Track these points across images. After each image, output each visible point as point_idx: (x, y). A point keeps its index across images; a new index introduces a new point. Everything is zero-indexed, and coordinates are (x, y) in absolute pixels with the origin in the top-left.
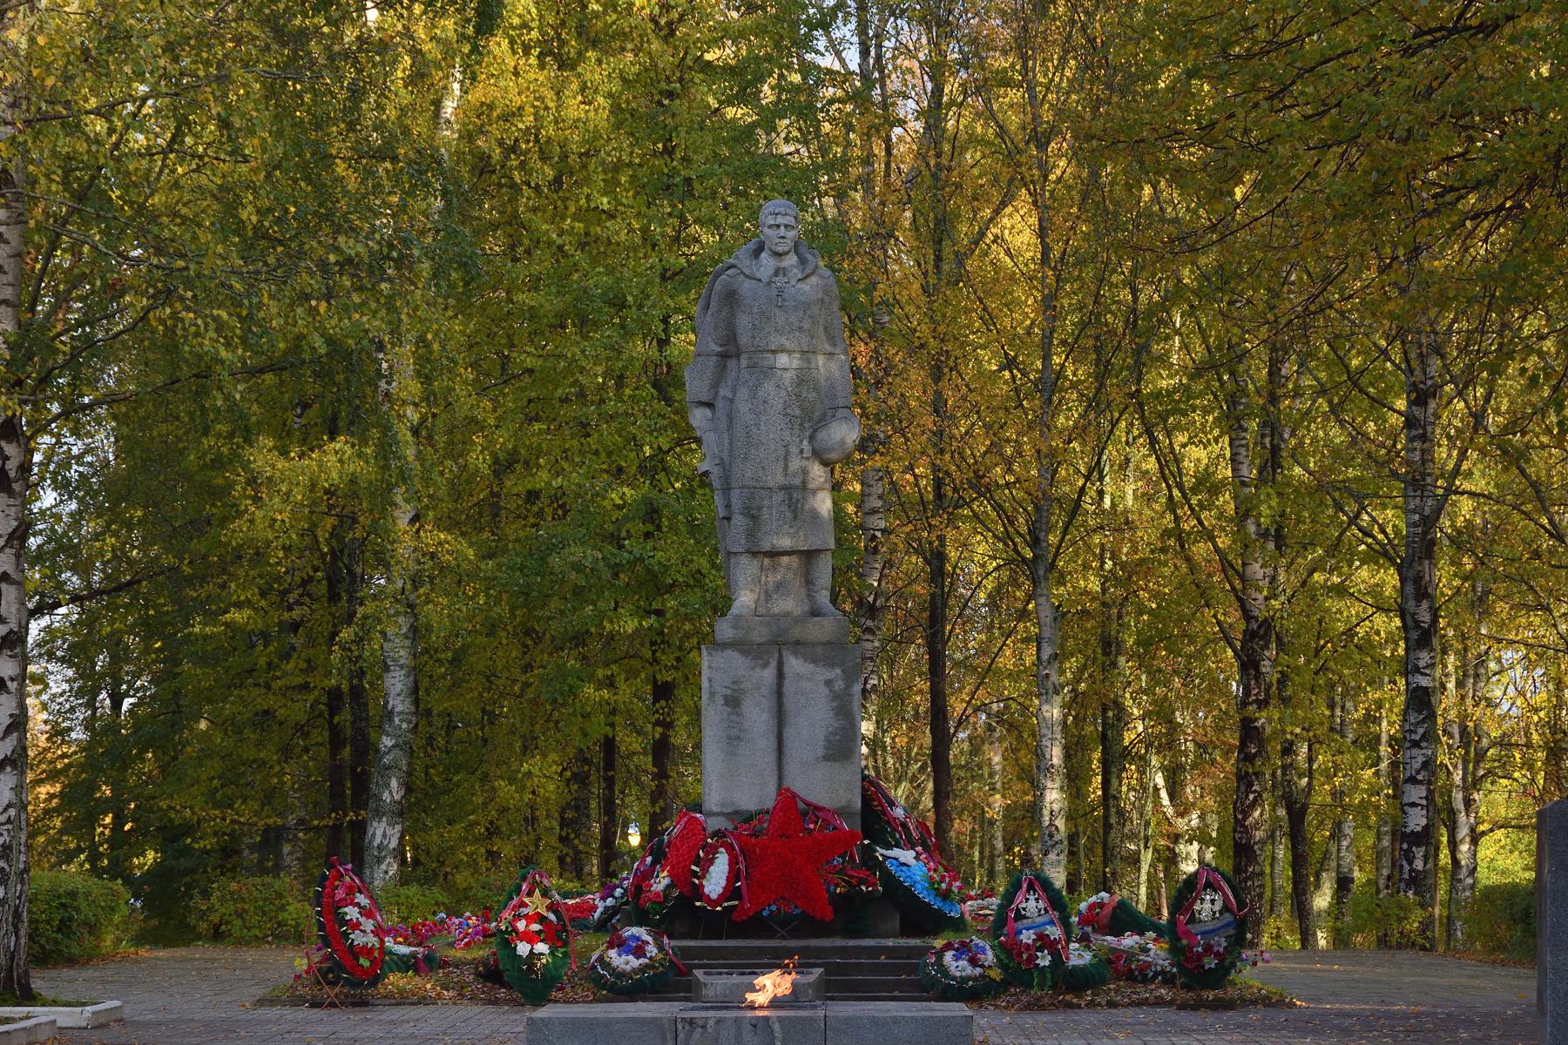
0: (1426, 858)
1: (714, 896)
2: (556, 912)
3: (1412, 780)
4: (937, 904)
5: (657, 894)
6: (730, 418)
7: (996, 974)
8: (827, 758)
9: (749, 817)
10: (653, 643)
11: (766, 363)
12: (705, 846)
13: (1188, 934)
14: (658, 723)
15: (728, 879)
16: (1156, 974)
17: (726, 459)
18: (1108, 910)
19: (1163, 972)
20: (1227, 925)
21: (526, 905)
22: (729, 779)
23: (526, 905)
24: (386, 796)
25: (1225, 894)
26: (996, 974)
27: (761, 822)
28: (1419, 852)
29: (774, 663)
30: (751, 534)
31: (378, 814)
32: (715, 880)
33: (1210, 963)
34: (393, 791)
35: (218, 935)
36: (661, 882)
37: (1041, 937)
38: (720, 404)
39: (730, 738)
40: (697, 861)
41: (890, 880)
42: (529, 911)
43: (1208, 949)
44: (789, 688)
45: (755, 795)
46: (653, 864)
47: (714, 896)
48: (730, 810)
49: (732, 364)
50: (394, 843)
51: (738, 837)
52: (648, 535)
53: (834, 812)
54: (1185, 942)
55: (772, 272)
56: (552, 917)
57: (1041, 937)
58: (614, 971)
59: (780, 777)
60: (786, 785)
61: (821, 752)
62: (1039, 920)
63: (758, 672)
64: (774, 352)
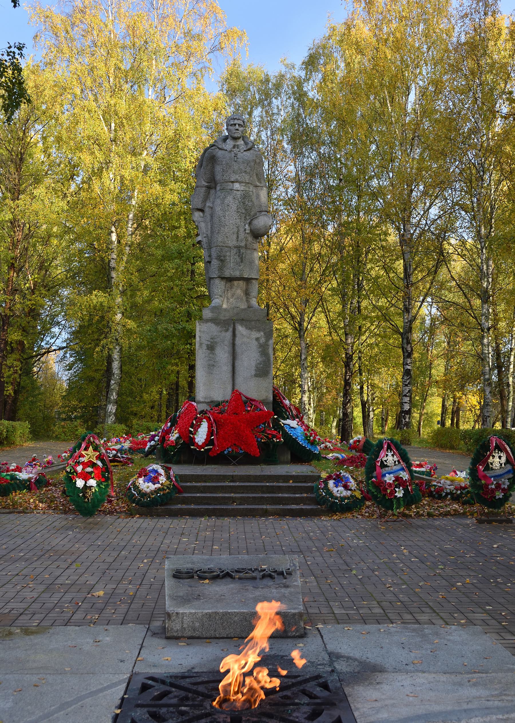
0: (409, 418)
1: (200, 443)
2: (102, 461)
3: (406, 396)
4: (309, 447)
5: (172, 442)
6: (212, 216)
7: (358, 494)
8: (256, 376)
9: (218, 404)
10: (189, 353)
11: (229, 187)
12: (196, 418)
13: (485, 477)
14: (189, 377)
15: (207, 435)
16: (447, 494)
17: (209, 235)
18: (362, 443)
19: (451, 493)
20: (508, 472)
21: (83, 456)
22: (210, 387)
23: (83, 456)
24: (112, 397)
25: (507, 452)
26: (358, 494)
27: (224, 407)
28: (407, 416)
29: (231, 329)
30: (221, 269)
31: (110, 403)
32: (201, 435)
33: (500, 495)
34: (114, 396)
35: (57, 438)
36: (174, 436)
37: (398, 479)
38: (207, 210)
39: (209, 365)
40: (192, 426)
41: (286, 435)
42: (85, 459)
43: (498, 486)
44: (238, 341)
45: (221, 393)
46: (171, 426)
47: (200, 443)
48: (209, 401)
49: (212, 191)
50: (114, 411)
51: (212, 414)
52: (187, 321)
53: (260, 402)
54: (483, 482)
55: (232, 146)
56: (99, 463)
57: (398, 479)
58: (140, 492)
59: (234, 385)
60: (236, 388)
61: (253, 373)
62: (395, 468)
63: (223, 334)
64: (233, 182)
